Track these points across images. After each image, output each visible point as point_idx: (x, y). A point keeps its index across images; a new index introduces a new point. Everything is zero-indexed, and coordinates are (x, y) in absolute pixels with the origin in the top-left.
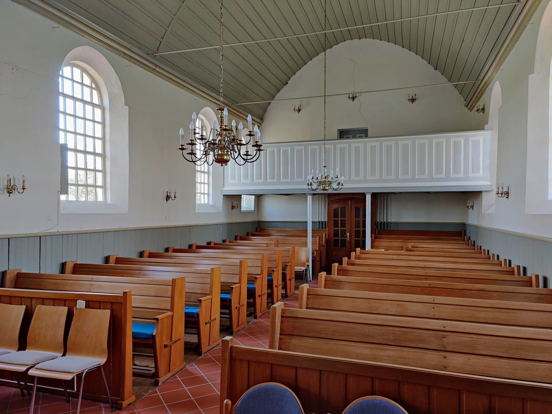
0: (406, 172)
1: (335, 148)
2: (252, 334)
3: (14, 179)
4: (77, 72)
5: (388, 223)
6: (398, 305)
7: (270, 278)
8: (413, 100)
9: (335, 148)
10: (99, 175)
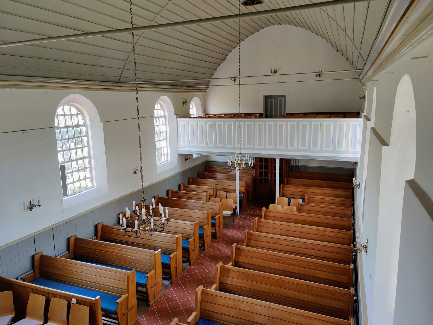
0: (304, 145)
1: (254, 124)
2: (184, 283)
3: (33, 200)
4: (66, 108)
5: (298, 167)
6: (250, 306)
7: (202, 232)
8: (320, 75)
9: (254, 124)
10: (86, 161)
